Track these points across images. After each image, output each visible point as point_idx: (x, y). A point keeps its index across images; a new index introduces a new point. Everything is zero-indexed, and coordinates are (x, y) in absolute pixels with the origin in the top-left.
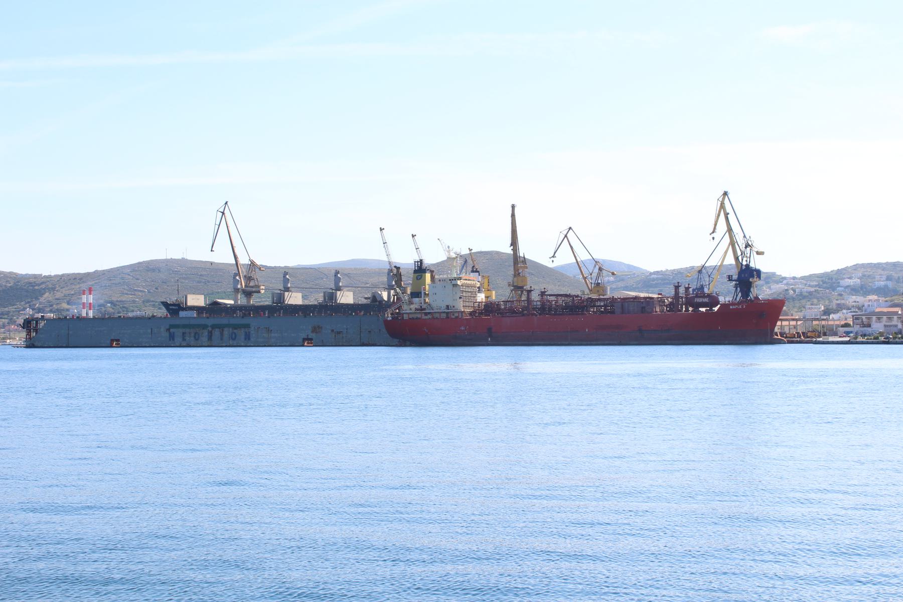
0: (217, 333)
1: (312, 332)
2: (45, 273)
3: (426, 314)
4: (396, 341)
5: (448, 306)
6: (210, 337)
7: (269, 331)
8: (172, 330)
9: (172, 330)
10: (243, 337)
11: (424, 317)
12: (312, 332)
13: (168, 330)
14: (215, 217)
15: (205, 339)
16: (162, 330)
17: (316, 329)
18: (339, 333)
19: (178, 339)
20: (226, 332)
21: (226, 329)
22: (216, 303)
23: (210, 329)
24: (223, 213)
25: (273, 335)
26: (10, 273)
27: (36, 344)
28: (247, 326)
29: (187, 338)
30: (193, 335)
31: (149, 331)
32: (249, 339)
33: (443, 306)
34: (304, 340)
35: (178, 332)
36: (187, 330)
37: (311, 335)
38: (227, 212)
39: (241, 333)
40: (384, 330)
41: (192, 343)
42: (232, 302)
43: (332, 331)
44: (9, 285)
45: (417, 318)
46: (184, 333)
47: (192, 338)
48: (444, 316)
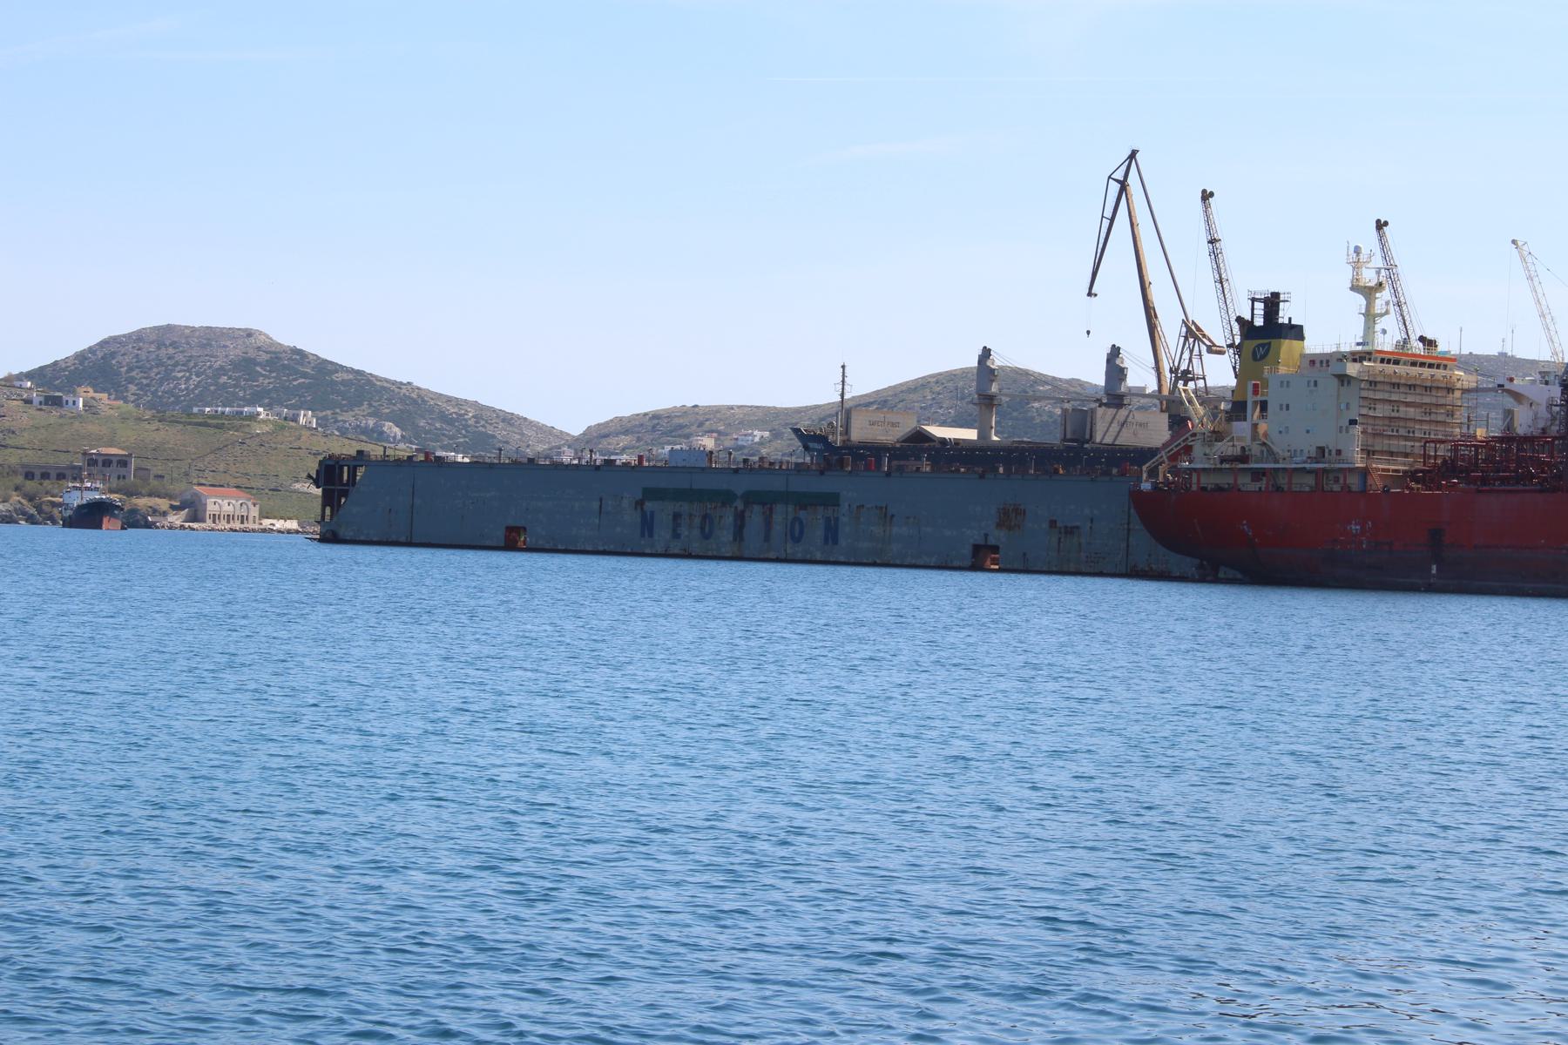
0: (755, 517)
1: (999, 525)
2: (221, 325)
3: (1257, 474)
4: (1175, 561)
5: (1321, 450)
6: (832, 533)
7: (886, 517)
8: (649, 505)
9: (649, 505)
10: (819, 533)
11: (1246, 483)
12: (999, 525)
13: (640, 504)
14: (1094, 196)
15: (725, 536)
16: (625, 503)
17: (1010, 517)
18: (1070, 531)
19: (662, 534)
20: (781, 515)
21: (779, 508)
22: (920, 437)
23: (740, 505)
24: (1124, 186)
25: (895, 530)
26: (1071, 382)
27: (344, 532)
28: (831, 500)
29: (684, 531)
30: (697, 521)
31: (596, 505)
32: (835, 542)
33: (1308, 446)
34: (978, 549)
35: (662, 511)
36: (685, 507)
37: (997, 536)
38: (1133, 179)
39: (815, 521)
40: (1137, 525)
41: (696, 547)
42: (970, 434)
43: (1053, 523)
44: (1481, 433)
45: (1219, 489)
46: (677, 516)
47: (696, 532)
48: (1310, 480)
